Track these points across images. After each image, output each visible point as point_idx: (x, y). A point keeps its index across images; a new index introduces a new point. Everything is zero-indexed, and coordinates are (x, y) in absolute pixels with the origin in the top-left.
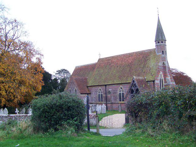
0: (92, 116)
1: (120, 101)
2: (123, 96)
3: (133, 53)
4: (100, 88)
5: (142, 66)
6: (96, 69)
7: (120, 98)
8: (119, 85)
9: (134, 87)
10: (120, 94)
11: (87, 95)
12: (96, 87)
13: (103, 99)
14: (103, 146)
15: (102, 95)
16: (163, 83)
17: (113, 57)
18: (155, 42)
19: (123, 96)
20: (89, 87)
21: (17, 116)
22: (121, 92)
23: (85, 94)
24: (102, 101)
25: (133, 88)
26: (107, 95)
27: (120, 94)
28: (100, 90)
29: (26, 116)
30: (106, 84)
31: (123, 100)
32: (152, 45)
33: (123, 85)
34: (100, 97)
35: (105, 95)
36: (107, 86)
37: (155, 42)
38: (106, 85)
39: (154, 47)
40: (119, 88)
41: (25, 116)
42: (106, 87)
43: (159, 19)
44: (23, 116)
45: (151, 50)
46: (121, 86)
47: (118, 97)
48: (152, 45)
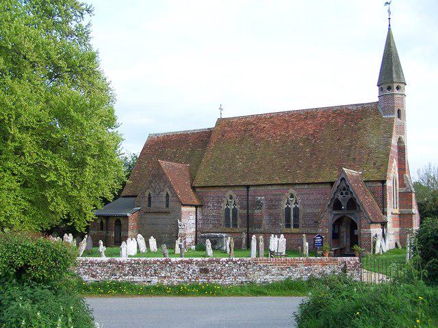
0: (349, 263)
1: (288, 226)
2: (296, 216)
3: (317, 109)
4: (230, 192)
5: (346, 142)
6: (212, 145)
7: (288, 220)
8: (285, 187)
9: (342, 194)
10: (288, 209)
11: (194, 209)
12: (220, 189)
13: (239, 221)
14: (111, 326)
15: (235, 210)
16: (398, 188)
17: (259, 118)
18: (378, 85)
19: (296, 216)
20: (198, 190)
21: (138, 263)
22: (292, 206)
23: (191, 206)
24: (235, 225)
25: (340, 197)
26: (250, 211)
27: (288, 209)
28: (231, 198)
29: (167, 261)
30: (250, 183)
31: (296, 226)
32: (369, 94)
33: (297, 187)
34: (231, 215)
35: (245, 212)
36: (252, 189)
37: (377, 88)
38: (248, 187)
39: (377, 100)
40: (286, 194)
41: (161, 262)
42: (248, 191)
43: (389, 29)
44: (155, 262)
45: (363, 104)
46: (291, 191)
47: (283, 218)
48: (369, 94)
